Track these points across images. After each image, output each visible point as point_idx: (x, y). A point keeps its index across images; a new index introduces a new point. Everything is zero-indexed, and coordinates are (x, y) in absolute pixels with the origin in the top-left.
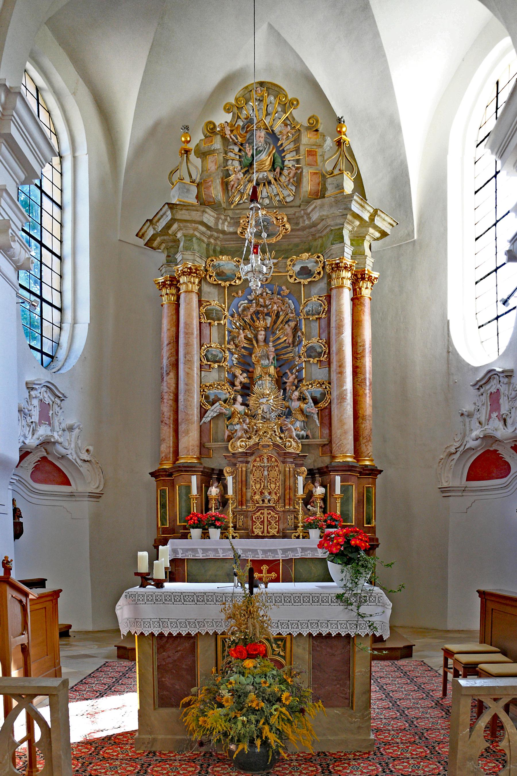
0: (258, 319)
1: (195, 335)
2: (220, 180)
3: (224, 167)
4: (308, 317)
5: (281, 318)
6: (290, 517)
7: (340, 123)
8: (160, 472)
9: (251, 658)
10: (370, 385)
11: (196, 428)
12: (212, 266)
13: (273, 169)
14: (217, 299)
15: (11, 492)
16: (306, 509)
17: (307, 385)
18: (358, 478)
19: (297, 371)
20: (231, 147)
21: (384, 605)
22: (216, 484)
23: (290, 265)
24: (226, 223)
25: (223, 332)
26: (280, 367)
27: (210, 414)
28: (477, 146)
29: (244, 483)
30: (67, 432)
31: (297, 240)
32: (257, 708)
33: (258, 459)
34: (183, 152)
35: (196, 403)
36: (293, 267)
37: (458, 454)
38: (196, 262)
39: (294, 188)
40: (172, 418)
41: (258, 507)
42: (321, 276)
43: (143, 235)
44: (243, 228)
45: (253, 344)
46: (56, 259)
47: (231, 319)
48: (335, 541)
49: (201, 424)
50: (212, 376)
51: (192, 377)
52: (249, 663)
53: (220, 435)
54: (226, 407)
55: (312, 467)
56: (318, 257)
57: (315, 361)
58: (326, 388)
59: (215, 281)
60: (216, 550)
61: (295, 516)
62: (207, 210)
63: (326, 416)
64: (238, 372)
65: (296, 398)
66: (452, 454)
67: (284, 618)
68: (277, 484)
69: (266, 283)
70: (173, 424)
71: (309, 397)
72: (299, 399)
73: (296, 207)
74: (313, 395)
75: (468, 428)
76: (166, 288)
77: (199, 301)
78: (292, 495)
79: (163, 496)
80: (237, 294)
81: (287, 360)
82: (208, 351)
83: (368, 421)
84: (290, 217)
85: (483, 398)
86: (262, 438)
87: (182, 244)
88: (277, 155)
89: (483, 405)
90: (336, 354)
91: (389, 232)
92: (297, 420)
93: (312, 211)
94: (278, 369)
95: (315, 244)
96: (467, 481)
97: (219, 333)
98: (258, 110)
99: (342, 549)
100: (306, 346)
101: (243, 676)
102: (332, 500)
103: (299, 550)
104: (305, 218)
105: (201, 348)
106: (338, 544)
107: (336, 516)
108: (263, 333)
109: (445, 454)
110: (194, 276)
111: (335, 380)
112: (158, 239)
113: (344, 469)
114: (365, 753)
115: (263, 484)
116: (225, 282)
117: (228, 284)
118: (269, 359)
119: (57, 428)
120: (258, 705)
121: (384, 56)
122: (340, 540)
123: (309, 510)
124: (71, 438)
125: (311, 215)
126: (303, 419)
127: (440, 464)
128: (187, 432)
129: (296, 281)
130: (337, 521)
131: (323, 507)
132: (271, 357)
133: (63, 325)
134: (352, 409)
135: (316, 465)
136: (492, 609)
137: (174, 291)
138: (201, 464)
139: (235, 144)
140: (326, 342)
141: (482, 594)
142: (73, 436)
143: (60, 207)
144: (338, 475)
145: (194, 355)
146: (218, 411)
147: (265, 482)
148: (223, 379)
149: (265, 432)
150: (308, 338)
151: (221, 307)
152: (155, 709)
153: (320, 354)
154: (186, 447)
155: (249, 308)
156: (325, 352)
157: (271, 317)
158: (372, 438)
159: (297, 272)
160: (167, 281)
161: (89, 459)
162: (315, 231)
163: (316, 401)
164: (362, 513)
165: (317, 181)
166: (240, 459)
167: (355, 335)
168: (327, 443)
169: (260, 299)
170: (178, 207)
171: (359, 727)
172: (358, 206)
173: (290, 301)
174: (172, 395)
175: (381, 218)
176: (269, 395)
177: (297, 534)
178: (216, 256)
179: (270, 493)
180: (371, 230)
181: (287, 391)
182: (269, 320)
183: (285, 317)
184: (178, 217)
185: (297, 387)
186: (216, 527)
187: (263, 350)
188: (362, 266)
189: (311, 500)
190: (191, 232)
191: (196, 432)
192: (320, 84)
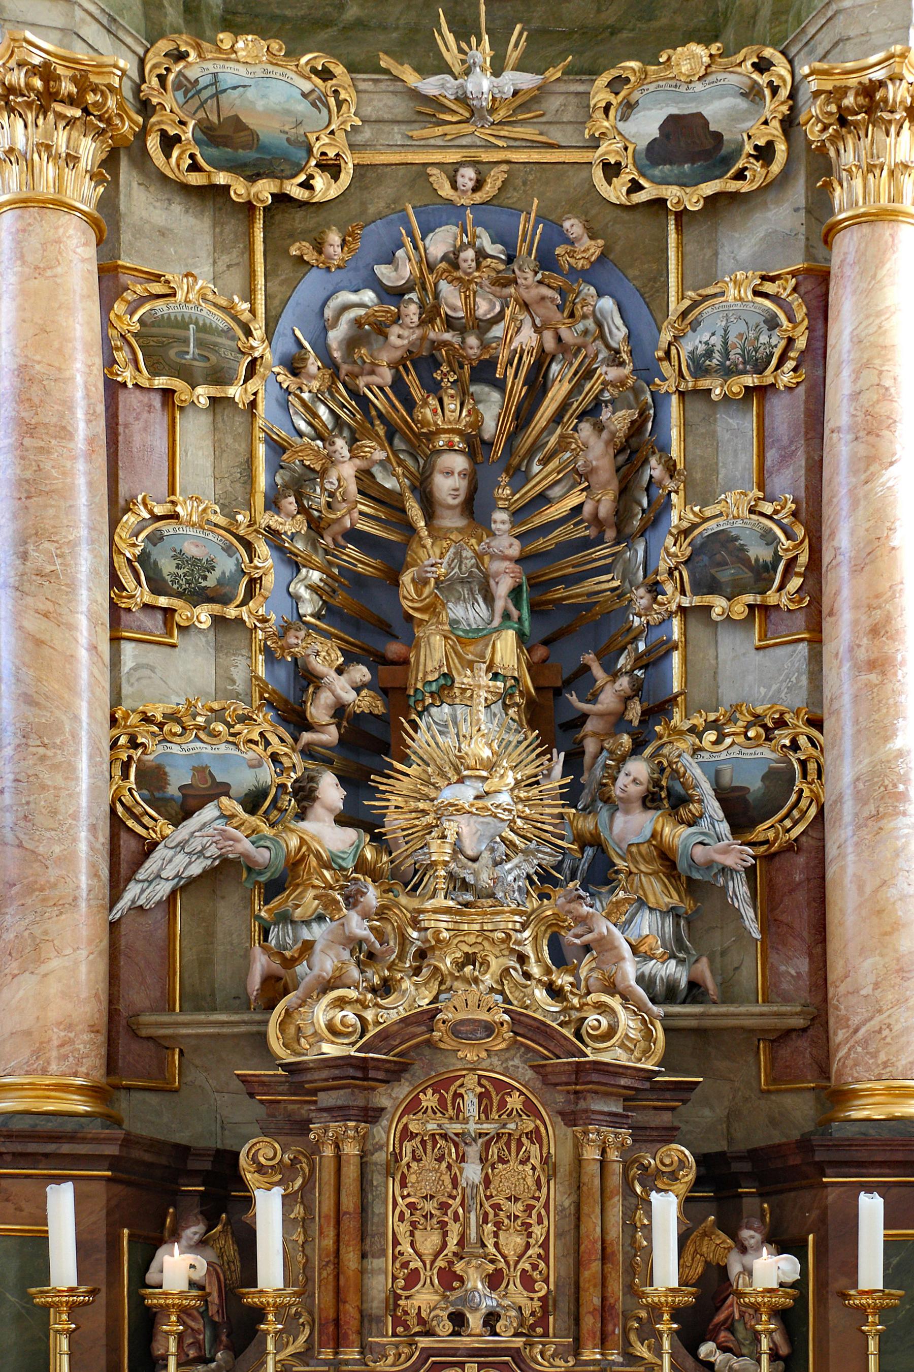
0: (434, 388)
4: (704, 384)
5: (557, 393)
11: (84, 932)
12: (178, 86)
17: (692, 730)
23: (607, 109)
25: (242, 447)
29: (350, 1225)
33: (429, 1100)
35: (84, 801)
36: (624, 118)
41: (427, 1353)
42: (776, 168)
47: (287, 381)
49: (116, 914)
53: (222, 973)
56: (762, 66)
57: (739, 610)
58: (795, 746)
59: (195, 167)
64: (324, 656)
65: (636, 791)
69: (479, 197)
71: (706, 788)
72: (650, 801)
74: (726, 780)
77: (102, 270)
78: (616, 1287)
80: (319, 247)
81: (589, 607)
82: (155, 539)
94: (541, 652)
97: (218, 450)
100: (686, 532)
102: (835, 1316)
105: (114, 523)
108: (459, 462)
110: (70, 122)
111: (846, 700)
113: (899, 1157)
115: (454, 1230)
116: (252, 178)
117: (265, 189)
118: (489, 599)
126: (675, 900)
129: (640, 197)
131: (784, 1350)
132: (502, 589)
140: (794, 514)
144: (869, 1188)
145: (73, 545)
146: (213, 851)
148: (240, 686)
149: (470, 959)
150: (702, 493)
153: (762, 576)
154: (28, 1033)
155: (381, 330)
156: (792, 562)
157: (499, 385)
159: (643, 144)
163: (741, 812)
166: (326, 1099)
169: (443, 285)
173: (607, 303)
176: (491, 766)
179: (494, 1281)
181: (587, 759)
182: (492, 410)
187: (458, 555)
189: (721, 1317)
191: (83, 953)
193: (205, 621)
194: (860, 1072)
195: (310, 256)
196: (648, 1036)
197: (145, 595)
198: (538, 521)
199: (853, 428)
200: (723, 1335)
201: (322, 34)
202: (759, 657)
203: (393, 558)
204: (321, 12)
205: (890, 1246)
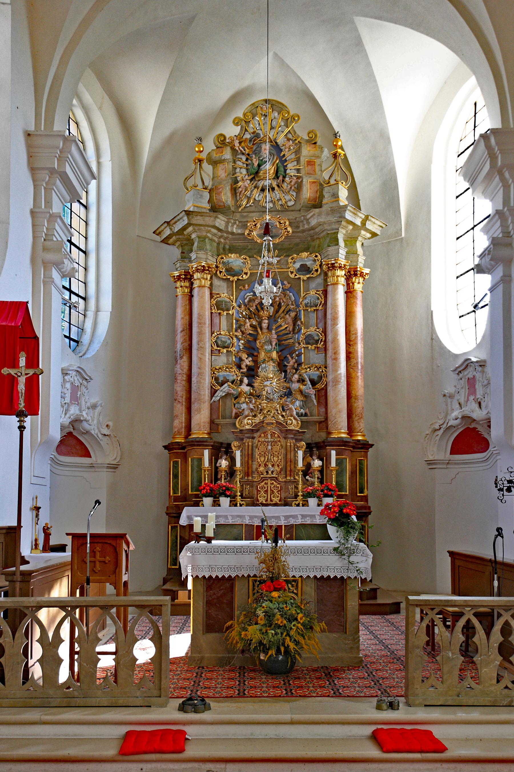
1: (207, 325)
2: (230, 187)
3: (233, 175)
4: (307, 308)
6: (291, 487)
7: (336, 137)
8: (173, 445)
9: (275, 591)
10: (362, 368)
13: (277, 177)
14: (226, 291)
15: (49, 465)
16: (305, 480)
18: (352, 451)
19: (297, 356)
20: (239, 156)
21: (367, 556)
22: (225, 457)
24: (235, 226)
25: (231, 321)
26: (281, 351)
27: (219, 394)
28: (458, 156)
29: (250, 456)
30: (91, 410)
31: (297, 240)
32: (281, 625)
33: (263, 435)
34: (197, 161)
35: (207, 385)
37: (442, 431)
38: (208, 261)
39: (294, 194)
40: (184, 397)
41: (262, 478)
42: (318, 273)
43: (160, 233)
45: (257, 331)
46: (82, 254)
47: (238, 309)
48: (332, 510)
50: (222, 360)
51: (205, 362)
52: (275, 594)
53: (228, 413)
54: (233, 388)
55: (310, 441)
57: (313, 348)
58: (322, 371)
59: (225, 276)
60: (226, 517)
61: (295, 486)
62: (219, 216)
63: (323, 396)
64: (244, 356)
65: (296, 380)
66: (436, 430)
67: (297, 565)
68: (280, 457)
70: (185, 402)
72: (298, 381)
73: (297, 211)
74: (311, 377)
75: (450, 408)
76: (181, 281)
78: (292, 467)
79: (175, 466)
80: (244, 287)
83: (360, 400)
84: (292, 221)
85: (462, 382)
86: (266, 417)
87: (196, 244)
88: (280, 164)
89: (462, 388)
90: (332, 343)
91: (378, 232)
92: (297, 399)
93: (311, 217)
94: (280, 353)
95: (313, 244)
96: (451, 454)
97: (227, 321)
98: (264, 124)
99: (337, 515)
101: (271, 603)
102: (328, 472)
103: (300, 517)
104: (305, 222)
105: (212, 336)
106: (334, 512)
107: (332, 486)
109: (430, 430)
112: (174, 237)
113: (339, 444)
114: (355, 667)
115: (267, 457)
116: (234, 277)
117: (236, 278)
118: (271, 345)
119: (84, 408)
120: (282, 622)
121: (375, 81)
122: (336, 509)
123: (308, 480)
124: (94, 415)
125: (310, 220)
126: (302, 399)
127: (426, 439)
128: (199, 410)
130: (332, 491)
131: (320, 477)
132: (274, 344)
133: (88, 313)
134: (345, 391)
135: (313, 439)
136: (459, 566)
137: (187, 284)
138: (211, 438)
139: (243, 154)
140: (322, 331)
141: (452, 554)
142: (96, 414)
143: (86, 207)
144: (333, 449)
147: (269, 456)
148: (230, 362)
149: (269, 411)
150: (307, 328)
151: (230, 298)
152: (203, 634)
153: (317, 342)
155: (254, 300)
156: (322, 340)
158: (364, 415)
160: (181, 275)
161: (109, 434)
162: (314, 233)
163: (314, 383)
164: (355, 483)
165: (316, 189)
166: (247, 435)
167: (348, 323)
168: (323, 420)
170: (194, 214)
171: (352, 648)
172: (351, 214)
173: (291, 294)
174: (185, 376)
175: (372, 222)
176: (272, 378)
177: (297, 503)
178: (226, 254)
179: (273, 466)
180: (363, 232)
183: (286, 307)
184: (194, 221)
185: (297, 370)
186: (227, 496)
187: (266, 337)
188: (355, 264)
189: (310, 472)
190: (204, 234)
192: (319, 101)
194: (332, 429)
195: (243, 289)
196: (298, 423)
197: (216, 347)
198: (279, 330)
199: (331, 319)
200: (310, 475)
202: (316, 355)
203: (255, 338)
205: (337, 459)
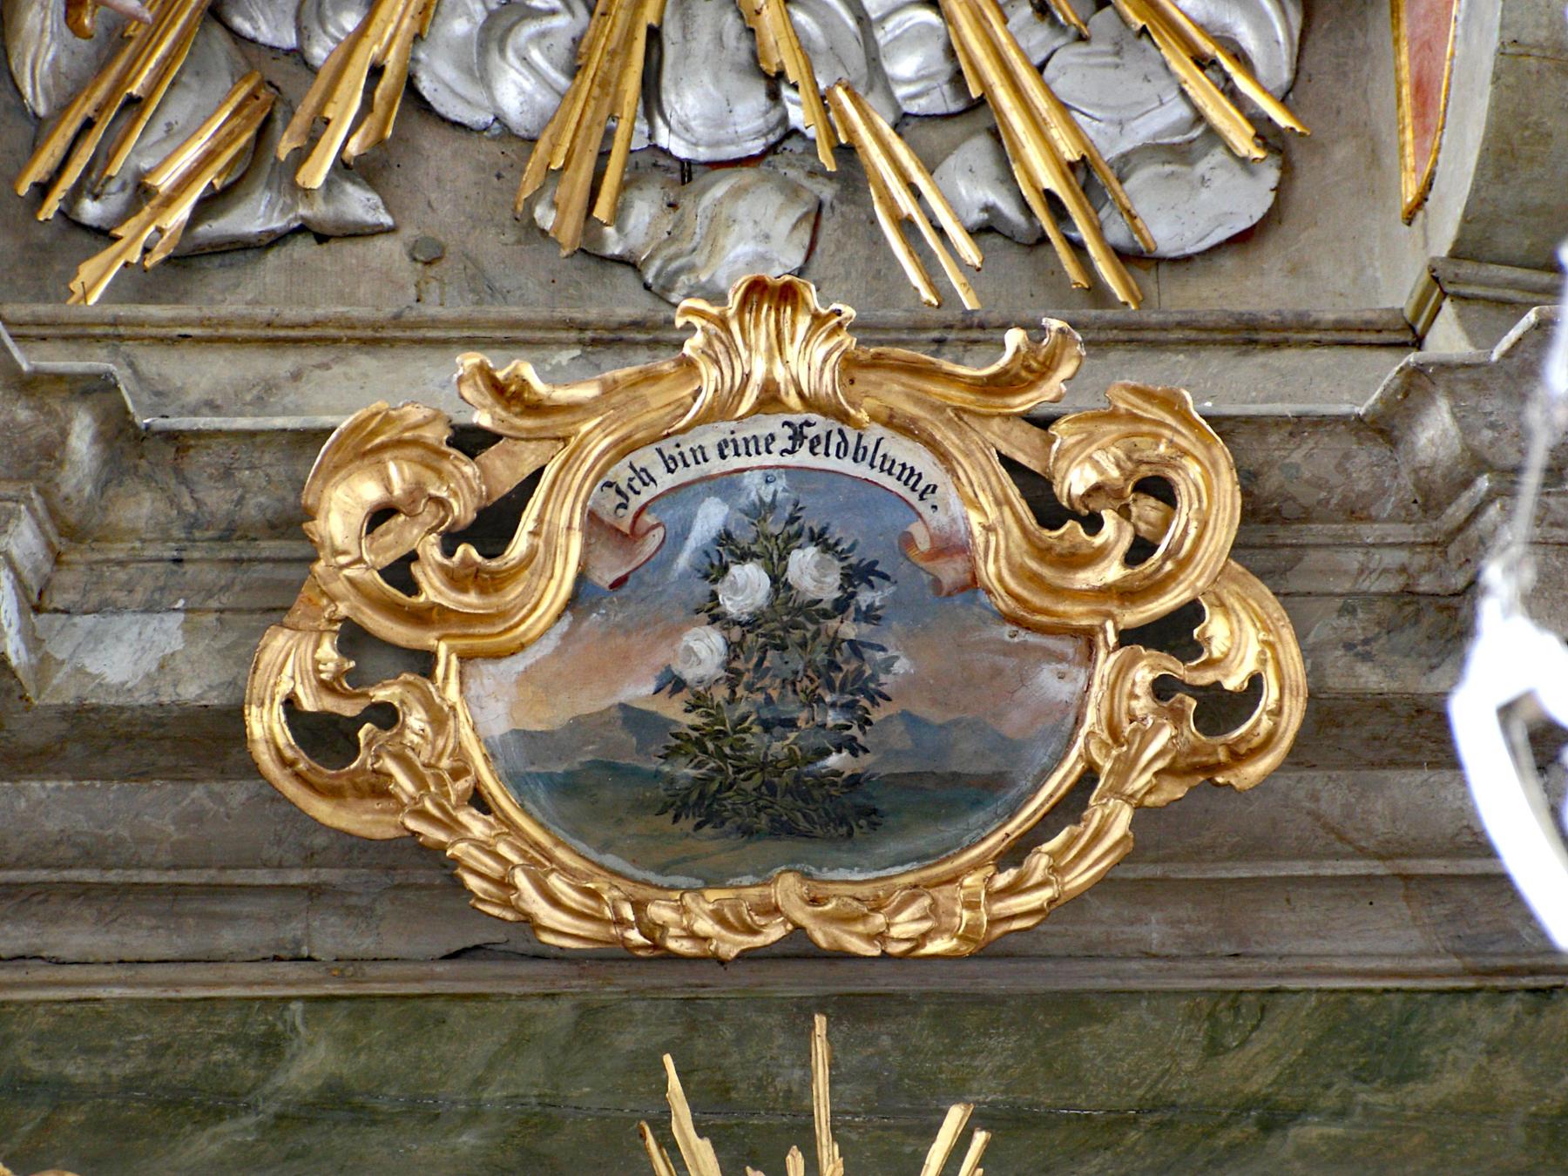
44: (353, 638)
84: (1305, 466)
193: (667, 367)
201: (202, 1139)
204: (196, 1065)
